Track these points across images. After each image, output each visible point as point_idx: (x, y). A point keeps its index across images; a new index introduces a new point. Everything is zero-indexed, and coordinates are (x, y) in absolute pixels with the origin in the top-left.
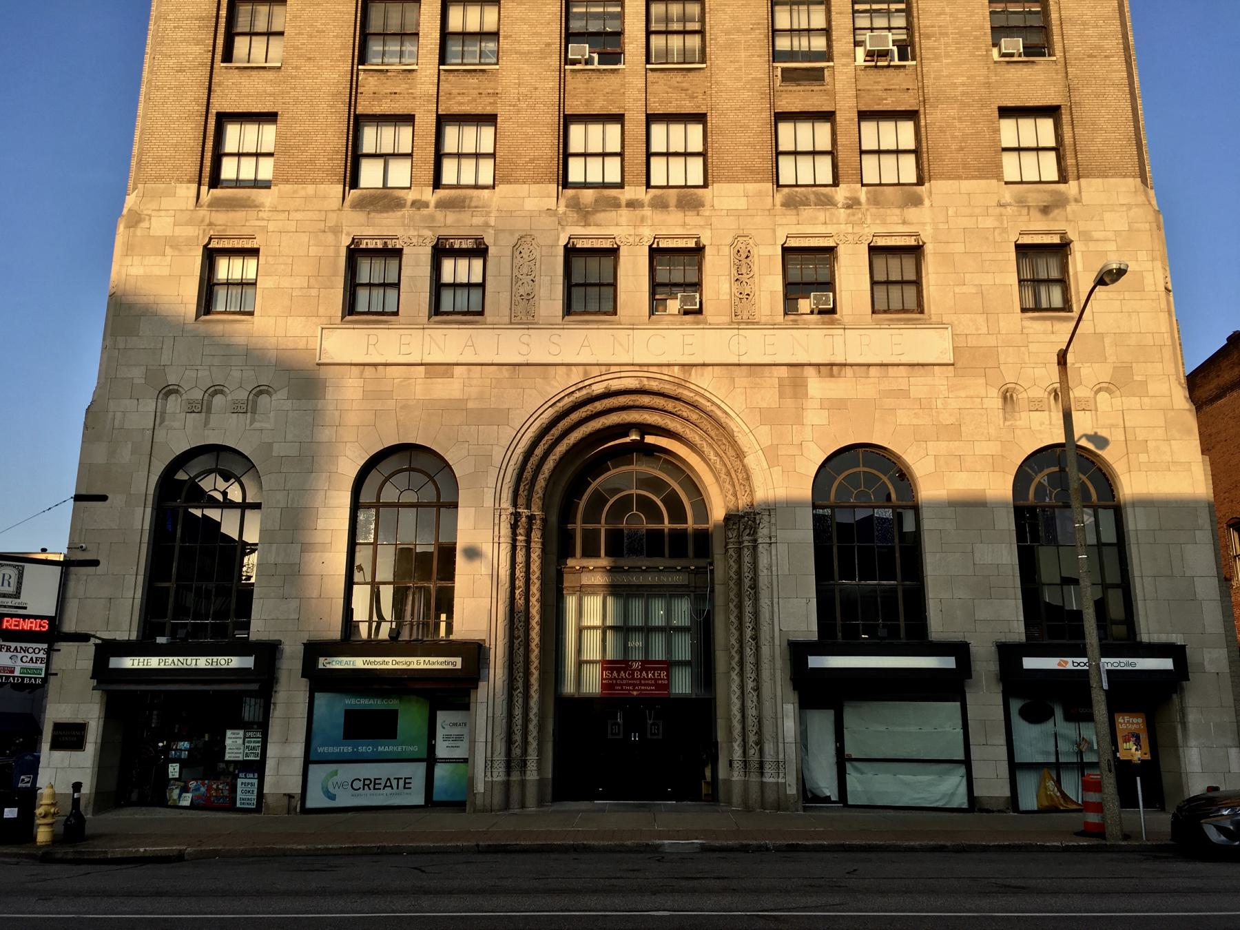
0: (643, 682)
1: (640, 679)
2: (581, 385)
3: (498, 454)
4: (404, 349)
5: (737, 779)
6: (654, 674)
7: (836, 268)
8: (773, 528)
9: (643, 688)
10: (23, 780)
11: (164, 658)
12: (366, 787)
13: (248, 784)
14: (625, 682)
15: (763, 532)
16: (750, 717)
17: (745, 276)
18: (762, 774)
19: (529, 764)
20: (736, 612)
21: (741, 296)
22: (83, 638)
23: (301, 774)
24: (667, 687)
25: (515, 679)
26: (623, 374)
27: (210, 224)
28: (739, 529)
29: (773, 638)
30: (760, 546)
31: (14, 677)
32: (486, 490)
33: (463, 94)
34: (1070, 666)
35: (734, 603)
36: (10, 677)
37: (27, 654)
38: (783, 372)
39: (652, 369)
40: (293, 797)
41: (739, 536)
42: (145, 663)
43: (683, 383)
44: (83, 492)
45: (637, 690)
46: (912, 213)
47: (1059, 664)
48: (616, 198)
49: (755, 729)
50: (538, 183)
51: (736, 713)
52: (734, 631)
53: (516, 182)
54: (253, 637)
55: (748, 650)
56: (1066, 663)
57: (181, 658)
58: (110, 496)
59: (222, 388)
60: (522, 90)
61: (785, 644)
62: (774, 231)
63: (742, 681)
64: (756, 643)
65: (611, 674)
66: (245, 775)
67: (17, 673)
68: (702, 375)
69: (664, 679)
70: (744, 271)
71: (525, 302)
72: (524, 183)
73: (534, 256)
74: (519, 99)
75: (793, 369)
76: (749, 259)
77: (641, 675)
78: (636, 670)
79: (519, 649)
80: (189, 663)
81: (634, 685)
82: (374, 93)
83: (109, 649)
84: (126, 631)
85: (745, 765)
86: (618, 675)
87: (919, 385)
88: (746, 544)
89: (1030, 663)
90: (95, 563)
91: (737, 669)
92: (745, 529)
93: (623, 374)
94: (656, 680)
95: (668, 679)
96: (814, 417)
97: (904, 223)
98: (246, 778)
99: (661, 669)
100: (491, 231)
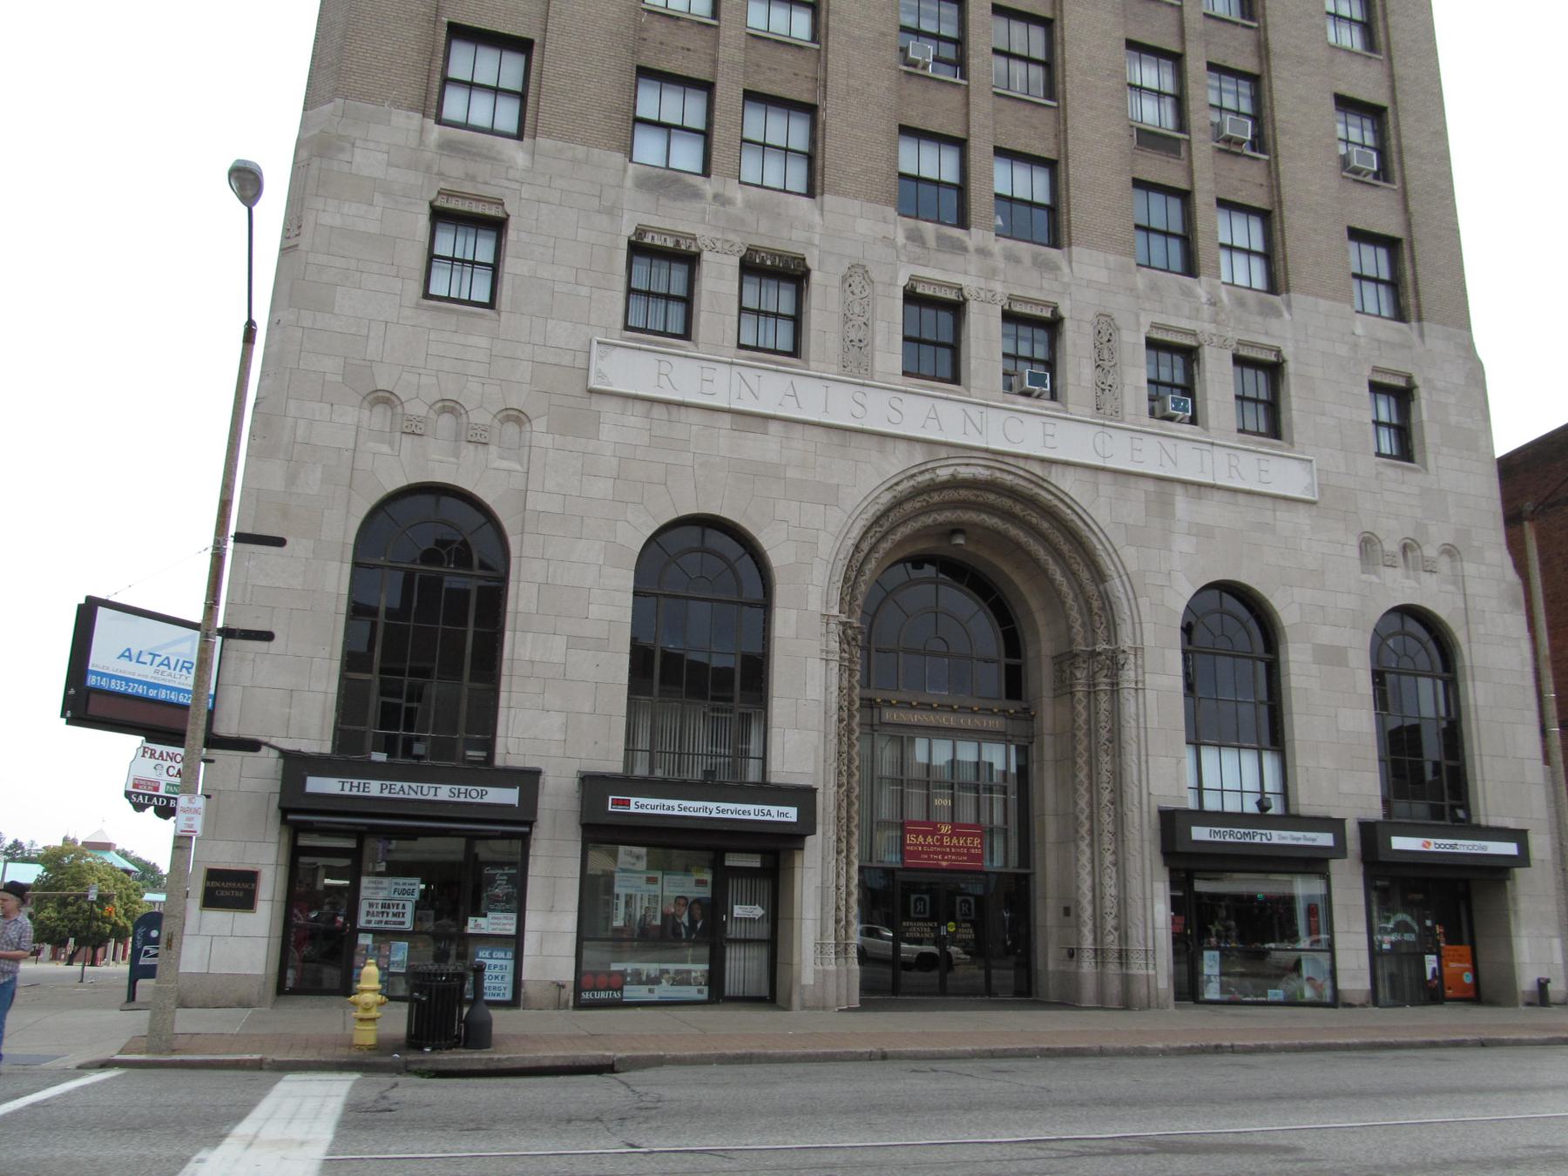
0: (953, 850)
1: (949, 846)
2: (923, 468)
4: (707, 387)
7: (1196, 371)
8: (1140, 671)
10: (147, 952)
11: (388, 783)
13: (495, 967)
14: (932, 849)
15: (1129, 675)
16: (1108, 897)
17: (1106, 363)
18: (1147, 969)
21: (1103, 386)
22: (253, 746)
23: (574, 954)
26: (973, 461)
27: (440, 174)
28: (1088, 668)
29: (1140, 803)
30: (1125, 691)
31: (158, 797)
33: (775, 69)
34: (1432, 848)
36: (153, 796)
37: (174, 764)
38: (1150, 486)
39: (1007, 460)
41: (1092, 676)
42: (361, 789)
43: (1041, 482)
44: (249, 531)
45: (947, 860)
46: (1274, 324)
47: (1424, 846)
48: (962, 242)
49: (1114, 911)
50: (872, 202)
53: (845, 194)
55: (1106, 816)
56: (1429, 843)
57: (414, 785)
58: (290, 540)
60: (852, 82)
61: (1155, 813)
62: (1137, 316)
65: (917, 838)
66: (491, 954)
67: (162, 792)
68: (1063, 475)
69: (976, 848)
70: (1106, 357)
71: (856, 350)
72: (856, 198)
73: (867, 293)
74: (848, 93)
76: (1111, 343)
80: (425, 792)
81: (944, 854)
82: (662, 43)
83: (296, 765)
84: (317, 739)
86: (925, 841)
87: (1286, 519)
89: (1399, 843)
90: (267, 636)
92: (1101, 669)
93: (973, 461)
94: (968, 848)
96: (1183, 544)
97: (1266, 333)
98: (492, 958)
99: (973, 835)
100: (816, 252)
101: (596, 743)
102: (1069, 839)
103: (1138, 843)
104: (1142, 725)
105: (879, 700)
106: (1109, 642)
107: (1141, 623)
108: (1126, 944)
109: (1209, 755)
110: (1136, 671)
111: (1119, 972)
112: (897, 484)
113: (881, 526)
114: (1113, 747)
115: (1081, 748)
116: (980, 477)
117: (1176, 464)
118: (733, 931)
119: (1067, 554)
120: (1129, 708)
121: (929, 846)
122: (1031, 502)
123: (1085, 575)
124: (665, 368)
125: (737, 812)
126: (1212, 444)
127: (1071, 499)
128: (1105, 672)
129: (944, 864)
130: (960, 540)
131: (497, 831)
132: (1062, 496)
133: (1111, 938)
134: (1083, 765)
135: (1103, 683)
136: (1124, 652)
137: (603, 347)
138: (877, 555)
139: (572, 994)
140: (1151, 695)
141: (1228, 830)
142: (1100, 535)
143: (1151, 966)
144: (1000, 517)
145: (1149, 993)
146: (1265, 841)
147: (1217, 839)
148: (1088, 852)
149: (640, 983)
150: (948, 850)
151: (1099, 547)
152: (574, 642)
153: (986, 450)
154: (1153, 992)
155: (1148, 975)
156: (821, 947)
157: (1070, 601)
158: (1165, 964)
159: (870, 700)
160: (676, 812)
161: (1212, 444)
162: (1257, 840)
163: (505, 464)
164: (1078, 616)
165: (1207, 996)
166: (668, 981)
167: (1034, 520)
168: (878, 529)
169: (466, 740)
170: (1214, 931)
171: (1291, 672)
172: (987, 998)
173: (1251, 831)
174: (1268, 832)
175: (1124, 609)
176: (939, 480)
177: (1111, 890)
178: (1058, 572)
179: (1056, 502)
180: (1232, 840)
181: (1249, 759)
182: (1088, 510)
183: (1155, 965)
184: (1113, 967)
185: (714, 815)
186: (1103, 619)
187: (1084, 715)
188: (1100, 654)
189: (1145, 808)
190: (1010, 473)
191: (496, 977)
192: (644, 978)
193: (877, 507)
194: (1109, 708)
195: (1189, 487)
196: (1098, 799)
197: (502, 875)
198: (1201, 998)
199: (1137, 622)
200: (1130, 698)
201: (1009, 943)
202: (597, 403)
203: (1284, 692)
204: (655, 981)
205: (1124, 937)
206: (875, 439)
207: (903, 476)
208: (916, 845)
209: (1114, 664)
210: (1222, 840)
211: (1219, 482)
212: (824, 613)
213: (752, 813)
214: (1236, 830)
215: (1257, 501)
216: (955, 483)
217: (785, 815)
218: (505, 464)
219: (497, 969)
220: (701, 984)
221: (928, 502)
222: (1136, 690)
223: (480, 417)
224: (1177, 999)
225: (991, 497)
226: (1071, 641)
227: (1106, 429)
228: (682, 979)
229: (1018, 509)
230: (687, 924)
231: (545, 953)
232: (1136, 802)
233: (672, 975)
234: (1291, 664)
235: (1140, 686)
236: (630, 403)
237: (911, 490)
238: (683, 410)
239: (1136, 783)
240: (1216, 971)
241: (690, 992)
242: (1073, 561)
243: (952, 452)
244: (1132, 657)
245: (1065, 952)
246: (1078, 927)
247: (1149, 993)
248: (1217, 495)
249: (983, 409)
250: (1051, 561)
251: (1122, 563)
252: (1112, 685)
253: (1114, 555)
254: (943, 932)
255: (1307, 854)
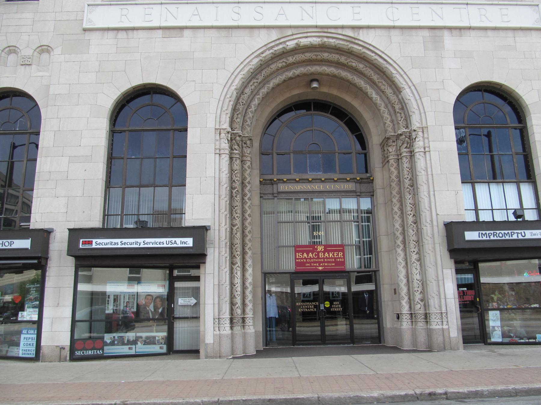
0: (326, 260)
1: (324, 258)
2: (278, 42)
3: (218, 90)
5: (405, 327)
6: (333, 254)
8: (426, 141)
9: (326, 264)
12: (495, 236)
13: (29, 338)
14: (312, 260)
15: (419, 144)
16: (415, 281)
18: (442, 325)
19: (246, 320)
20: (398, 205)
24: (343, 263)
25: (234, 256)
26: (309, 34)
28: (397, 145)
29: (432, 221)
30: (417, 154)
32: (208, 115)
35: (397, 198)
38: (426, 33)
39: (330, 30)
40: (64, 349)
43: (353, 40)
45: (321, 266)
49: (420, 289)
51: (403, 278)
52: (398, 219)
54: (32, 227)
59: (14, 48)
61: (441, 226)
63: (406, 255)
64: (417, 226)
65: (302, 255)
66: (27, 332)
69: (341, 258)
75: (433, 31)
77: (324, 255)
78: (320, 252)
79: (236, 234)
81: (320, 263)
85: (412, 317)
86: (308, 256)
88: (404, 154)
91: (402, 246)
92: (403, 144)
93: (309, 34)
94: (335, 258)
95: (344, 258)
98: (28, 334)
101: (84, 212)
102: (392, 249)
103: (431, 246)
104: (430, 173)
105: (275, 180)
106: (407, 127)
107: (425, 113)
108: (429, 310)
109: (481, 189)
110: (424, 141)
111: (425, 327)
112: (262, 53)
113: (257, 79)
114: (414, 189)
115: (394, 192)
116: (315, 43)
117: (442, 19)
118: (178, 313)
119: (377, 81)
120: (420, 163)
121: (311, 258)
122: (350, 53)
123: (389, 91)
124: (125, 12)
125: (156, 243)
126: (467, 4)
127: (374, 47)
128: (405, 145)
129: (320, 268)
130: (315, 85)
131: (20, 263)
132: (368, 46)
133: (418, 306)
134: (396, 203)
135: (404, 151)
136: (415, 131)
137: (91, 7)
138: (258, 96)
139: (69, 352)
140: (434, 155)
141: (492, 232)
142: (394, 65)
143: (445, 323)
144: (335, 67)
145: (444, 340)
146: (520, 237)
147: (484, 238)
148: (402, 254)
149: (123, 344)
150: (322, 260)
151: (394, 72)
152: (73, 159)
153: (316, 27)
154: (447, 340)
155: (443, 329)
156: (218, 320)
157: (382, 108)
158: (455, 321)
159: (271, 180)
160: (119, 246)
161: (467, 4)
162: (515, 237)
163: (40, 74)
164: (388, 116)
165: (493, 340)
166: (141, 343)
167: (354, 65)
168: (255, 81)
169: (21, 217)
170: (495, 298)
171: (535, 131)
172: (352, 345)
173: (510, 232)
174: (522, 231)
175: (413, 106)
176: (288, 48)
177: (416, 276)
178: (374, 93)
179: (365, 50)
180: (495, 238)
181: (511, 189)
182: (385, 52)
183: (447, 322)
184: (421, 325)
185: (142, 246)
186: (403, 115)
187: (395, 173)
188: (401, 135)
189: (435, 223)
190: (333, 38)
191: (30, 344)
192: (126, 342)
193: (250, 67)
194: (409, 166)
195: (453, 31)
196: (407, 222)
197: (33, 288)
198: (489, 341)
199: (423, 113)
200: (421, 158)
201: (368, 312)
202: (88, 35)
203: (532, 145)
204: (135, 342)
205: (426, 306)
206: (247, 31)
207: (265, 48)
208: (302, 259)
209: (410, 139)
210: (488, 238)
211: (473, 25)
212: (217, 127)
213: (165, 243)
214: (498, 232)
215: (502, 33)
216: (298, 50)
217: (185, 243)
218: (40, 74)
219: (30, 340)
220: (162, 343)
221: (286, 63)
222: (425, 152)
223: (27, 52)
224: (464, 343)
225: (326, 55)
226: (386, 131)
227: (394, 5)
228: (150, 341)
229: (343, 59)
230: (153, 310)
231: (53, 330)
232: (428, 221)
233: (144, 339)
234: (534, 127)
235: (427, 149)
236: (106, 32)
237: (272, 55)
238: (135, 32)
239: (428, 209)
240: (498, 323)
241: (155, 349)
242: (381, 84)
243: (295, 31)
244: (420, 134)
245: (395, 316)
246: (399, 300)
247: (444, 340)
248: (473, 33)
249: (314, 5)
250: (355, 78)
251: (410, 79)
252: (411, 152)
253: (404, 76)
254: (322, 308)
255: (125, 93)
